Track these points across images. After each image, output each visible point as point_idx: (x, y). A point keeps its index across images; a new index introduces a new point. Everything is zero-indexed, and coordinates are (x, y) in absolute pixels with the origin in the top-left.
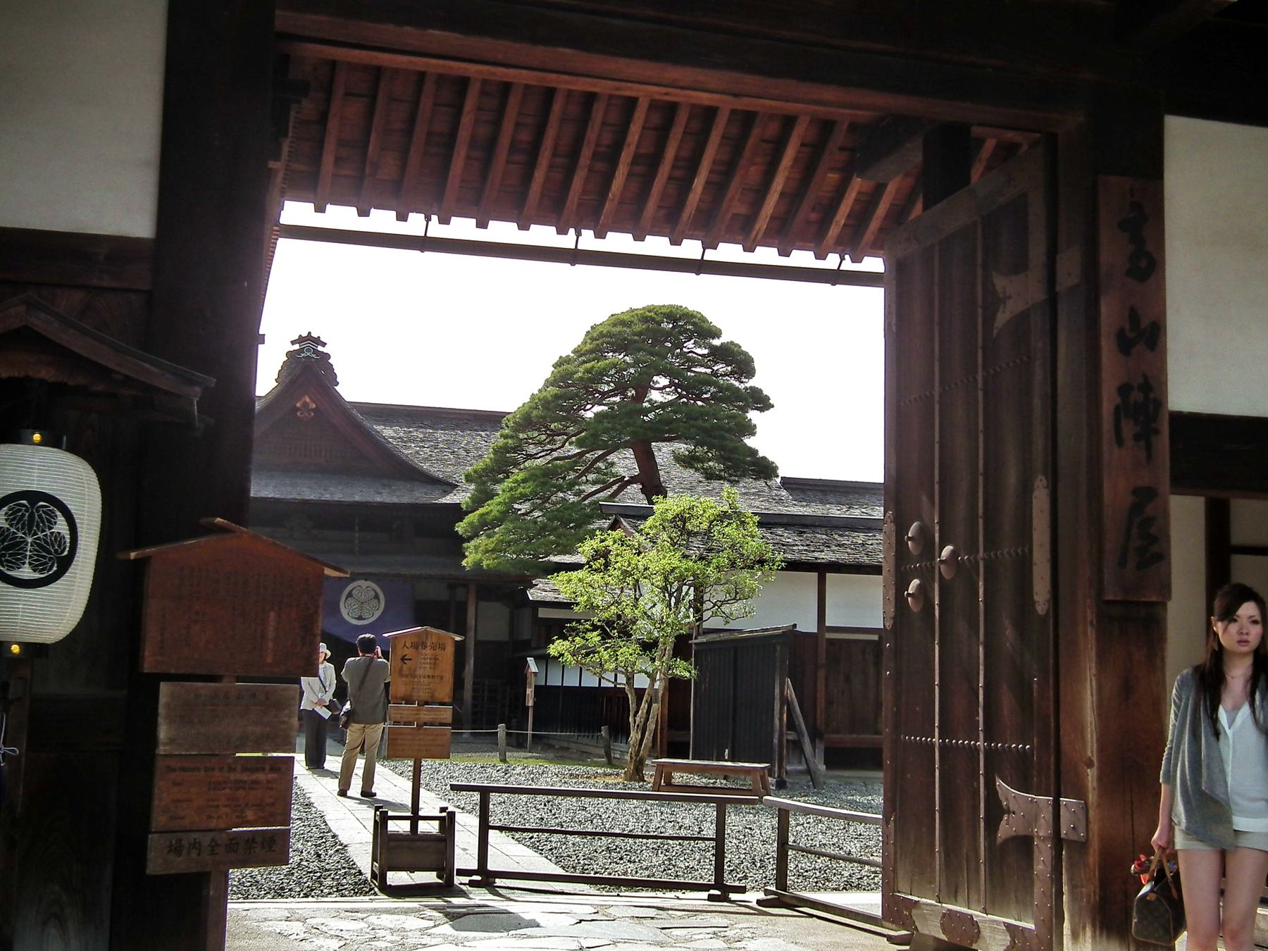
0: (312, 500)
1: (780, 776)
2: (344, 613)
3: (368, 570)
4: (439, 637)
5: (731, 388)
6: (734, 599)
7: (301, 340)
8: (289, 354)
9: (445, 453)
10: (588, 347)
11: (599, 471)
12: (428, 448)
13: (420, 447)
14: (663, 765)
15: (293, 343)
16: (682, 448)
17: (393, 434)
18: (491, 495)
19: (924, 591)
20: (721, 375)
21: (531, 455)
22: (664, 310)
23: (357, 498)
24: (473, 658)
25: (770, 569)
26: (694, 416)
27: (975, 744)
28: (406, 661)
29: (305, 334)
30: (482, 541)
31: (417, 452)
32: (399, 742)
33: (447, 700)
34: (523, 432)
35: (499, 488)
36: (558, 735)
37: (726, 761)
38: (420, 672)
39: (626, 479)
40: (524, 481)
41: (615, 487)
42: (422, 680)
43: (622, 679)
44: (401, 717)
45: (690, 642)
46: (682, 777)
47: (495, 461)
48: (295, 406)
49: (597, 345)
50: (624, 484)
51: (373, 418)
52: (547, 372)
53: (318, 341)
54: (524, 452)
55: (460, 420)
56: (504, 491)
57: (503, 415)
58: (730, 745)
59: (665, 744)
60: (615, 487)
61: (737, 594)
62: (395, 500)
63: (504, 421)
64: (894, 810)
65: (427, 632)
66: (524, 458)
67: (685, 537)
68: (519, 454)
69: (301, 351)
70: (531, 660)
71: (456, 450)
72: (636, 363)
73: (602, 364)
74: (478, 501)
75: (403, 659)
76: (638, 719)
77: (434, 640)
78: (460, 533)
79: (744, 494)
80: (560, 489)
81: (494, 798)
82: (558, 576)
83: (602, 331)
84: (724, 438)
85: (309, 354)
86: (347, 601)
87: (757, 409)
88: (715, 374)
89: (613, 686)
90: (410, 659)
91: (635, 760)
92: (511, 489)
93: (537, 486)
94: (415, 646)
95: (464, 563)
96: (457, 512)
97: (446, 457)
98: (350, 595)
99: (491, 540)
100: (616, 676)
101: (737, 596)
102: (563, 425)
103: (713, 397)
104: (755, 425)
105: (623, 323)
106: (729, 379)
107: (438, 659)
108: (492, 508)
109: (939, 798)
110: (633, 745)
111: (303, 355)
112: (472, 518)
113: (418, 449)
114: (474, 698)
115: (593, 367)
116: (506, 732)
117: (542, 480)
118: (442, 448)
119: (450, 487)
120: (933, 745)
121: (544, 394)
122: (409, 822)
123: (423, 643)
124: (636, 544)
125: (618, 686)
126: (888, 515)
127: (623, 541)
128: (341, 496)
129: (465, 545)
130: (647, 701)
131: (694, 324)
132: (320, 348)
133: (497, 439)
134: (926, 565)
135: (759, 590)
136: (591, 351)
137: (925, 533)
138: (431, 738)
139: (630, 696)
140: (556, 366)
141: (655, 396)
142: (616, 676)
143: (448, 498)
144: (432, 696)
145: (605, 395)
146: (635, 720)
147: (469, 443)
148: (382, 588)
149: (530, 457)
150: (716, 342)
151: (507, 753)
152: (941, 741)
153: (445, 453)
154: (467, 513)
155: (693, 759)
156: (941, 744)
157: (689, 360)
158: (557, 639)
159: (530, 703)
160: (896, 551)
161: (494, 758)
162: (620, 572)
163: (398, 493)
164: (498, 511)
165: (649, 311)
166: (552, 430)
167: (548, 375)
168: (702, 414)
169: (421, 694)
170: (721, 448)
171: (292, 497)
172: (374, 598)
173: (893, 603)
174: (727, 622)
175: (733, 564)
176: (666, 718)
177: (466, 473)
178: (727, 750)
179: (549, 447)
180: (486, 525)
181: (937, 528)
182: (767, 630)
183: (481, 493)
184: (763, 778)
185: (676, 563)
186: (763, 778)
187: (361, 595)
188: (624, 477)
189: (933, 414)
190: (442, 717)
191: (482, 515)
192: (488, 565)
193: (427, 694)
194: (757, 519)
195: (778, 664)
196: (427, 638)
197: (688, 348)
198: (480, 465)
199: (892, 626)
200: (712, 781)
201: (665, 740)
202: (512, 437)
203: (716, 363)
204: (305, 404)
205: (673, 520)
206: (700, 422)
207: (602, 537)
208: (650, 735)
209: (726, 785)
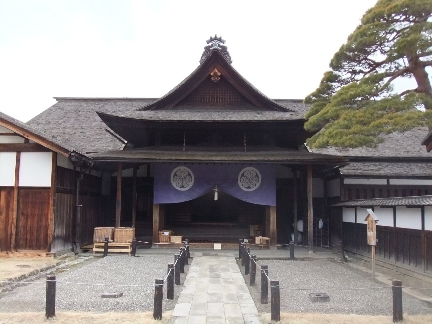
2: (240, 184)
7: (212, 40)
24: (312, 207)
29: (213, 37)
53: (220, 40)
85: (216, 47)
98: (189, 175)
128: (235, 118)
148: (259, 171)
204: (215, 74)
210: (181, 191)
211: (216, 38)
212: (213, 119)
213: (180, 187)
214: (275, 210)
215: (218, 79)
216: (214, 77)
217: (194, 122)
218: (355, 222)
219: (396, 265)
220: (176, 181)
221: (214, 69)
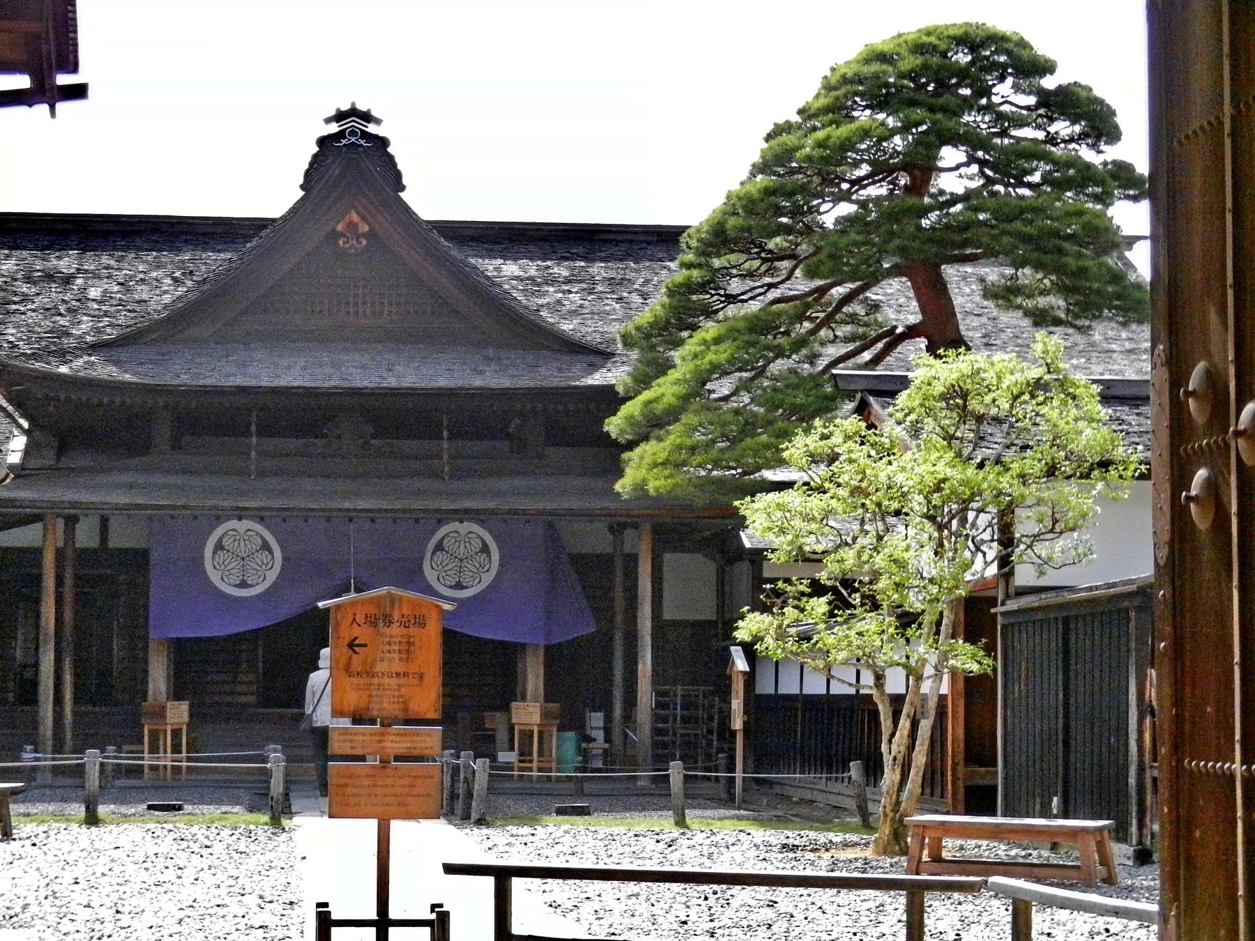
0: (366, 388)
1: (1140, 842)
3: (469, 504)
4: (414, 604)
5: (1075, 162)
6: (1052, 531)
7: (340, 116)
8: (323, 142)
9: (606, 301)
10: (823, 102)
11: (853, 319)
12: (577, 293)
13: (564, 292)
14: (924, 827)
15: (328, 121)
16: (994, 273)
17: (518, 272)
18: (664, 367)
19: (1214, 488)
20: (1064, 141)
21: (735, 297)
22: (952, 32)
23: (442, 382)
25: (1121, 477)
26: (1008, 214)
27: (1229, 768)
28: (357, 649)
29: (345, 107)
30: (648, 450)
31: (559, 302)
32: (349, 790)
33: (431, 715)
34: (719, 256)
35: (676, 355)
36: (795, 778)
37: (1056, 817)
38: (381, 667)
39: (899, 331)
40: (717, 341)
41: (880, 345)
42: (386, 680)
43: (868, 678)
44: (352, 748)
45: (993, 610)
46: (980, 847)
47: (672, 309)
48: (334, 230)
49: (837, 98)
50: (894, 339)
51: (486, 246)
52: (754, 149)
53: (367, 117)
54: (722, 292)
55: (632, 242)
56: (683, 359)
57: (682, 229)
58: (1060, 789)
59: (961, 791)
60: (880, 345)
61: (1056, 526)
62: (506, 383)
63: (683, 239)
64: (1176, 899)
65: (392, 598)
66: (722, 302)
67: (971, 424)
68: (713, 296)
69: (341, 135)
70: (736, 651)
71: (625, 294)
72: (905, 129)
73: (845, 130)
74: (643, 381)
75: (351, 645)
76: (894, 747)
77: (406, 610)
78: (613, 436)
79: (1130, 351)
80: (780, 353)
81: (517, 883)
82: (753, 501)
83: (845, 74)
84: (1060, 251)
85: (353, 139)
86: (435, 558)
87: (1128, 197)
88: (1052, 140)
89: (852, 691)
90: (365, 645)
91: (893, 819)
92: (696, 356)
93: (738, 348)
94: (372, 622)
95: (618, 487)
96: (610, 399)
97: (608, 308)
98: (439, 547)
99: (662, 444)
100: (858, 672)
101: (1057, 526)
102: (790, 242)
103: (1046, 179)
104: (1118, 227)
105: (883, 57)
106: (1077, 147)
107: (413, 644)
108: (666, 389)
109: (1244, 873)
110: (888, 792)
111: (344, 142)
112: (632, 408)
113: (560, 295)
114: (657, 718)
115: (828, 138)
116: (685, 776)
117: (746, 338)
118: (601, 292)
119: (599, 355)
120: (1232, 776)
121: (748, 187)
122: (373, 930)
123: (385, 616)
124: (887, 441)
125: (862, 692)
126: (1156, 352)
127: (864, 437)
129: (625, 456)
130: (908, 716)
131: (1009, 53)
132: (372, 129)
133: (674, 272)
134: (1216, 442)
135: (1095, 513)
136: (827, 110)
137: (1214, 380)
138: (406, 782)
139: (880, 707)
140: (769, 138)
141: (950, 183)
142: (858, 672)
143: (597, 376)
144: (406, 710)
145: (858, 183)
146: (892, 749)
147: (647, 282)
149: (731, 299)
150: (1049, 83)
151: (687, 811)
152: (1244, 767)
153: (606, 301)
154: (624, 400)
155: (1004, 815)
156: (1246, 774)
157: (1001, 117)
158: (749, 611)
159: (737, 724)
160: (1172, 420)
161: (664, 823)
162: (848, 490)
163: (512, 371)
164: (673, 395)
165: (929, 33)
166: (770, 251)
167: (756, 158)
168: (1020, 211)
169: (385, 705)
170: (1060, 270)
171: (332, 383)
172: (443, 549)
173: (1168, 516)
174: (1042, 573)
175: (1051, 471)
176: (962, 745)
177: (622, 331)
178: (1055, 799)
179: (768, 280)
180: (653, 424)
181: (1232, 370)
182: (1114, 585)
183: (648, 366)
184: (1101, 845)
185: (943, 470)
186: (1101, 845)
187: (459, 547)
188: (895, 327)
189: (1223, 159)
190: (424, 745)
191: (648, 403)
192: (657, 489)
193: (396, 706)
194: (1096, 389)
195: (1133, 645)
196: (392, 607)
197: (1003, 97)
198: (645, 317)
199: (1168, 558)
200: (1023, 853)
201: (960, 784)
202: (699, 266)
203: (1052, 120)
204: (352, 226)
205: (943, 397)
206: (1018, 225)
207: (826, 431)
208: (917, 775)
209: (1048, 858)
210: (237, 600)
211: (353, 112)
212: (345, 384)
213: (236, 586)
214: (541, 658)
215: (360, 243)
216: (346, 236)
217: (287, 391)
218: (824, 692)
219: (827, 789)
220: (223, 567)
221: (347, 212)
